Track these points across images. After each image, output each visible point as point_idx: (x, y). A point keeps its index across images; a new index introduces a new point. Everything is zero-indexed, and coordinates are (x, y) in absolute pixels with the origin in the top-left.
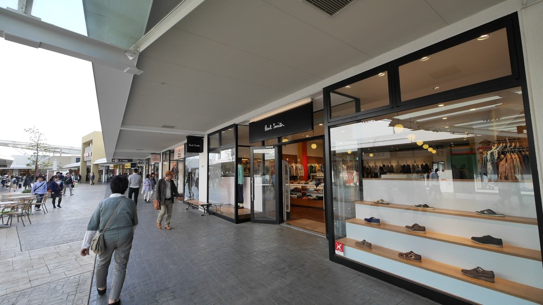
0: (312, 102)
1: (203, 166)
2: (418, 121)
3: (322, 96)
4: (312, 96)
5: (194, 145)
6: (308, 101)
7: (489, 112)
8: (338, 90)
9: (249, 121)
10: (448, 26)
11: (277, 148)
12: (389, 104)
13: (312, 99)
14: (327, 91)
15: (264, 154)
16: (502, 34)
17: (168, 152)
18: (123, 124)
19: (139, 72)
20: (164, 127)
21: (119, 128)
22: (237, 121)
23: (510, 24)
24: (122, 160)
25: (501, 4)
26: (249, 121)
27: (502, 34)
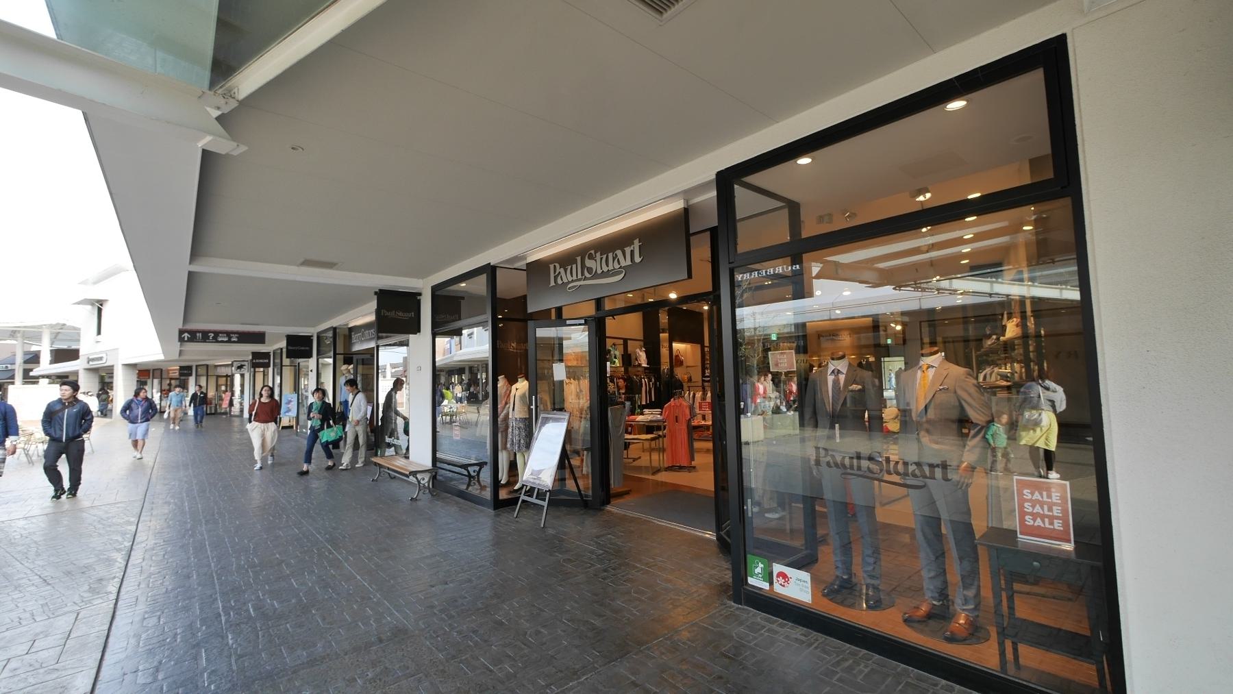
0: (686, 210)
1: (420, 369)
2: (882, 265)
3: (714, 193)
4: (687, 193)
5: (397, 315)
6: (678, 205)
7: (916, 267)
8: (753, 179)
9: (524, 258)
10: (776, 126)
11: (594, 324)
12: (1052, 176)
13: (687, 201)
14: (727, 180)
15: (561, 340)
16: (1034, 81)
17: (330, 334)
18: (195, 254)
19: (222, 145)
20: (307, 263)
21: (184, 266)
22: (494, 255)
23: (1051, 58)
24: (217, 333)
25: (1052, 5)
26: (524, 258)
27: (1034, 81)
